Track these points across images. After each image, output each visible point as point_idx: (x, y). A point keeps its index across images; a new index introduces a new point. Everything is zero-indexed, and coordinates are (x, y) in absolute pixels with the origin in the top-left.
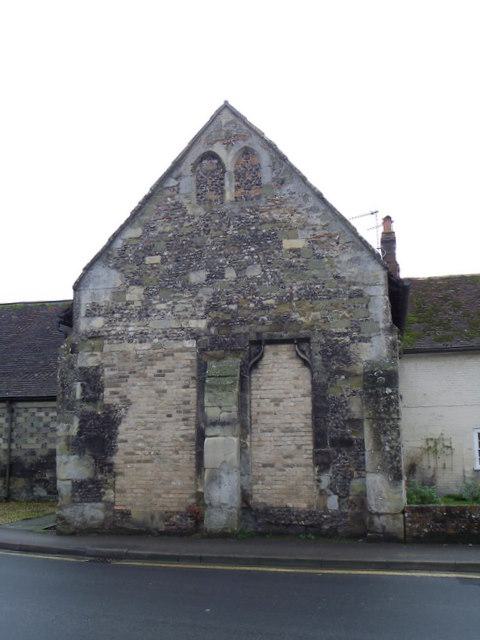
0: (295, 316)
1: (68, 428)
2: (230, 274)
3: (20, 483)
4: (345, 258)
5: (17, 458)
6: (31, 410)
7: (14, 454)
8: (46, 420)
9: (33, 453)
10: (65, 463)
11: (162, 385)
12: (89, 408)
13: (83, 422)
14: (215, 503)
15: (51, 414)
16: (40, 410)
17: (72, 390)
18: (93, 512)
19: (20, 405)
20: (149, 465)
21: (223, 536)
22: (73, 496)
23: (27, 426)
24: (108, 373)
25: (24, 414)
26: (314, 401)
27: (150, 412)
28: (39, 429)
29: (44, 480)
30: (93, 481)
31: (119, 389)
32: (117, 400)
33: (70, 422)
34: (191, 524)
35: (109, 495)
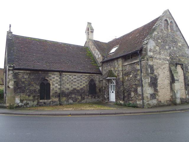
0: (181, 59)
1: (148, 80)
2: (172, 48)
3: (64, 99)
4: (186, 49)
5: (63, 91)
6: (67, 75)
7: (62, 89)
8: (72, 79)
9: (68, 89)
10: (148, 89)
11: (164, 71)
12: (152, 75)
13: (151, 79)
14: (177, 98)
15: (74, 77)
16: (70, 75)
17: (148, 70)
18: (154, 102)
19: (64, 73)
20: (163, 89)
21: (179, 104)
22: (151, 98)
23: (66, 80)
24: (155, 67)
25: (66, 77)
26: (184, 76)
27: (163, 77)
28: (70, 82)
29: (72, 98)
30: (154, 94)
31: (157, 71)
32: (157, 74)
33: (148, 79)
34: (173, 102)
35: (157, 97)
